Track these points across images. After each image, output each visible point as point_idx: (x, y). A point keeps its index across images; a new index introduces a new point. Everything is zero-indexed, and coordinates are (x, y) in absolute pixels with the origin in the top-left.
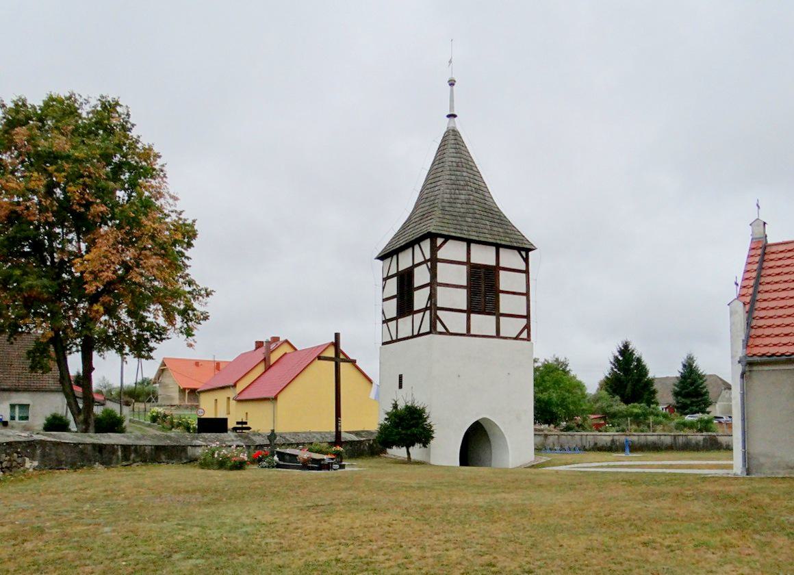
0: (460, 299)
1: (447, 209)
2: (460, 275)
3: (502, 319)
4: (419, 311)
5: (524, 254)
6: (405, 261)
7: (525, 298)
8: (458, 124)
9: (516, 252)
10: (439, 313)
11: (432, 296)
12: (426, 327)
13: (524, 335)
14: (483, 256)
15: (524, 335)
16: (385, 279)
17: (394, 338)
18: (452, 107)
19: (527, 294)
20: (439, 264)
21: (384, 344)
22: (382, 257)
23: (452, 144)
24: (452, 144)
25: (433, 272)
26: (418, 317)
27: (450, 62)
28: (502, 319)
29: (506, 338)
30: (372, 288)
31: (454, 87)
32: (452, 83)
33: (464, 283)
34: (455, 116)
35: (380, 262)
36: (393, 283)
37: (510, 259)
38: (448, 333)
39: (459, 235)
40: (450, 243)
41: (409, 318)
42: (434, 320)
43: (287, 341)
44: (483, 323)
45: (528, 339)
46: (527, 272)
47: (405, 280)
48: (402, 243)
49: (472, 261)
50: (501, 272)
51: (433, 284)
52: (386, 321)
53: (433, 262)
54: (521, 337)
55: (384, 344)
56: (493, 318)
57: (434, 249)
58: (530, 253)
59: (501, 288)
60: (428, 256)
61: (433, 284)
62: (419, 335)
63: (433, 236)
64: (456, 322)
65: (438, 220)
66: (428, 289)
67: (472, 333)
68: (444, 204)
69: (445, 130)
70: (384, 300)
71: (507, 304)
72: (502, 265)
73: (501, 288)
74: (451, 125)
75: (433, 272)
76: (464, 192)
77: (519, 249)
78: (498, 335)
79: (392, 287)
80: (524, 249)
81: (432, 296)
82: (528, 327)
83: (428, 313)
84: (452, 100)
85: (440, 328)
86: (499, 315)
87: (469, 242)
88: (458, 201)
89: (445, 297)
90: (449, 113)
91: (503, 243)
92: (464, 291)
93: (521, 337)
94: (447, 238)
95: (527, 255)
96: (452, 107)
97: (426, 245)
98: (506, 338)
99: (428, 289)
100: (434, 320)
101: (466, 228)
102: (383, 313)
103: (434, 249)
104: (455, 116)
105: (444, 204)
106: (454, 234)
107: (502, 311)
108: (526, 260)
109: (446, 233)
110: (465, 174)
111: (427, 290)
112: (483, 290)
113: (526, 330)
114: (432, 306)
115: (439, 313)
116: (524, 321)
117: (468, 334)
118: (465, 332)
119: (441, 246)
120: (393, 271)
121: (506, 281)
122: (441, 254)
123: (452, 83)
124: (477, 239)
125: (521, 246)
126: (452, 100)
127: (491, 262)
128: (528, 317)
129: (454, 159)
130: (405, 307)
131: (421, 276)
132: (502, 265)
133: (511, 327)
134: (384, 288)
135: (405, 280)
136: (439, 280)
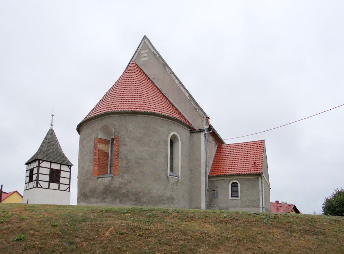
0: (47, 178)
1: (45, 152)
2: (48, 172)
3: (60, 185)
4: (34, 181)
5: (69, 167)
6: (32, 166)
7: (69, 179)
8: (54, 128)
9: (67, 166)
10: (39, 182)
11: (38, 177)
12: (35, 186)
13: (68, 190)
14: (56, 167)
15: (68, 190)
16: (27, 171)
17: (27, 189)
18: (52, 123)
19: (70, 178)
20: (40, 168)
21: (25, 190)
22: (27, 164)
23: (51, 133)
24: (51, 133)
25: (38, 170)
26: (34, 182)
27: (53, 109)
28: (60, 185)
29: (51, 189)
30: (23, 171)
31: (53, 117)
32: (52, 116)
33: (49, 174)
34: (53, 125)
35: (26, 165)
36: (29, 171)
37: (64, 168)
38: (42, 187)
39: (47, 160)
40: (44, 162)
41: (31, 183)
42: (37, 183)
43: (16, 191)
44: (54, 185)
45: (69, 191)
46: (70, 172)
47: (31, 171)
48: (31, 161)
49: (52, 168)
50: (61, 172)
51: (38, 173)
52: (26, 183)
53: (39, 167)
54: (67, 190)
55: (25, 190)
56: (58, 185)
57: (39, 164)
58: (72, 167)
59: (49, 176)
60: (37, 166)
61: (38, 173)
62: (33, 188)
63: (39, 160)
64: (46, 185)
65: (41, 155)
66: (36, 174)
67: (69, 177)
68: (44, 151)
69: (49, 129)
70: (26, 177)
71: (62, 180)
72: (62, 169)
73: (61, 176)
74: (51, 128)
75: (38, 170)
76: (52, 148)
77: (68, 166)
78: (59, 189)
79: (28, 174)
80: (70, 166)
81: (38, 177)
82: (69, 188)
83: (36, 181)
84: (52, 121)
85: (39, 186)
86: (59, 184)
87: (51, 162)
88: (49, 150)
89: (41, 177)
90: (51, 124)
91: (62, 163)
92: (49, 176)
93: (67, 190)
94: (44, 161)
95: (71, 167)
96: (52, 123)
97: (37, 162)
98: (51, 189)
99: (36, 174)
100: (37, 183)
101: (50, 158)
102: (25, 181)
103: (39, 164)
104: (53, 125)
105: (44, 151)
106: (46, 160)
107: (49, 169)
108: (70, 169)
109: (43, 159)
110: (53, 142)
111: (36, 175)
112: (55, 177)
113: (41, 187)
114: (37, 180)
115: (39, 182)
116: (68, 186)
117: (49, 188)
118: (48, 188)
119: (41, 163)
120: (29, 169)
121: (62, 174)
122: (41, 165)
123: (52, 116)
124: (53, 161)
125: (68, 164)
126: (52, 121)
127: (59, 168)
128: (69, 185)
129: (50, 138)
130: (31, 180)
131: (35, 171)
132: (62, 169)
133: (63, 187)
134: (26, 173)
135: (31, 171)
136: (40, 172)
